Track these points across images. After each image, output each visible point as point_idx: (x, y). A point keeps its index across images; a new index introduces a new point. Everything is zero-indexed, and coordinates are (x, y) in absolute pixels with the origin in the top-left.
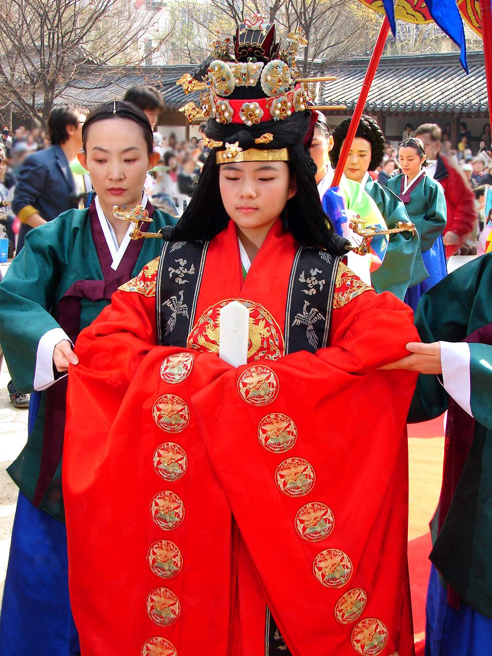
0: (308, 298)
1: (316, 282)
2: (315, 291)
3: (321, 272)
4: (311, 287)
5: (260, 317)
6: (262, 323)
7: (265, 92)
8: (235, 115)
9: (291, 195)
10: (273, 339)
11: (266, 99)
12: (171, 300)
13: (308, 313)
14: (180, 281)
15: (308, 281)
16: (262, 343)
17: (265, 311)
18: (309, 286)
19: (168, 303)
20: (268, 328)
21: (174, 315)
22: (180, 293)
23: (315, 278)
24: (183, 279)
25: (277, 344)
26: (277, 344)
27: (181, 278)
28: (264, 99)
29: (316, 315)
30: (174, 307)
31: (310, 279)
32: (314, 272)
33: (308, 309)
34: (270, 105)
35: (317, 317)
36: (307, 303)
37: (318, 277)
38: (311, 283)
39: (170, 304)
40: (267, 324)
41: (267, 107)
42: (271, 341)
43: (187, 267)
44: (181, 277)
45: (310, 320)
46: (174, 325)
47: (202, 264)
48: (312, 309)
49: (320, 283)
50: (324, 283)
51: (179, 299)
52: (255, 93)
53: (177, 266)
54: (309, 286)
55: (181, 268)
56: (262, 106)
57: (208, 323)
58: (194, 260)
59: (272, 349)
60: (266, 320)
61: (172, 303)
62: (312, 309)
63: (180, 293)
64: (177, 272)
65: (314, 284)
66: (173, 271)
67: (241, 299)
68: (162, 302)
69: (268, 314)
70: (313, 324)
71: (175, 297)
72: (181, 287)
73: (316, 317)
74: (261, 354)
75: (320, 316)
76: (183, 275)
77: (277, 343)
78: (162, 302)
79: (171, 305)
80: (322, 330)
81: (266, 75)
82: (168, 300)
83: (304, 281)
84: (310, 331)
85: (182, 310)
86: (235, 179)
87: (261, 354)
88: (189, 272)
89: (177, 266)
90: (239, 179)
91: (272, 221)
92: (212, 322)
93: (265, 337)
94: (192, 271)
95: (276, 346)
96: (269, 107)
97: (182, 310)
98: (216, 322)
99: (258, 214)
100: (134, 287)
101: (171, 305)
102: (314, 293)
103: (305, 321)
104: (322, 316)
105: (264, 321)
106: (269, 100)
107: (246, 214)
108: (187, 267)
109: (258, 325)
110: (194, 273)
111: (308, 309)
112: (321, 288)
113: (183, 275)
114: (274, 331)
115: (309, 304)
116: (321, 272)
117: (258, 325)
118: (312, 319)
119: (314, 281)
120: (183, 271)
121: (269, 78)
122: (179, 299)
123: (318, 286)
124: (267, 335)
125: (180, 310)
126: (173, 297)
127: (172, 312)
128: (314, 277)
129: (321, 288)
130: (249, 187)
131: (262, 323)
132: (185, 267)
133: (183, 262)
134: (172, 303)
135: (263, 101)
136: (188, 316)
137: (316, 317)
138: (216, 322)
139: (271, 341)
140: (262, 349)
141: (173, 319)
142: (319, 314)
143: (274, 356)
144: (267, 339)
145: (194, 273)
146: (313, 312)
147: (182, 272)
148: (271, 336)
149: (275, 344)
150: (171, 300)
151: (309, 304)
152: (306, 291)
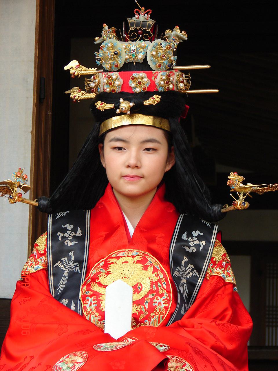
0: (188, 254)
1: (197, 242)
2: (195, 249)
3: (202, 234)
4: (192, 245)
5: (148, 263)
6: (151, 269)
7: (151, 66)
8: (125, 84)
9: (168, 168)
10: (161, 283)
11: (153, 71)
12: (62, 262)
13: (184, 268)
14: (70, 244)
15: (197, 242)
16: (151, 286)
17: (152, 258)
18: (190, 244)
19: (58, 264)
20: (156, 273)
21: (66, 274)
22: (70, 254)
23: (196, 239)
24: (71, 241)
25: (165, 287)
26: (165, 287)
27: (69, 240)
28: (151, 71)
29: (191, 271)
30: (65, 267)
31: (192, 239)
32: (196, 233)
33: (186, 266)
34: (156, 77)
35: (192, 273)
36: (185, 259)
37: (199, 238)
38: (193, 241)
39: (61, 265)
40: (155, 270)
41: (153, 78)
42: (159, 284)
43: (74, 230)
44: (70, 239)
45: (185, 274)
46: (66, 282)
47: (88, 226)
48: (190, 265)
49: (201, 243)
50: (204, 244)
51: (69, 260)
52: (143, 66)
53: (65, 230)
54: (190, 244)
55: (69, 232)
56: (149, 77)
57: (100, 273)
58: (79, 223)
59: (160, 292)
60: (154, 266)
61: (63, 264)
62: (190, 265)
63: (70, 254)
64: (65, 235)
65: (195, 243)
66: (62, 235)
67: (130, 249)
68: (54, 263)
69: (155, 261)
70: (187, 279)
71: (66, 259)
72: (70, 249)
73: (191, 273)
74: (150, 296)
75: (195, 273)
76: (72, 238)
77: (165, 286)
78: (54, 263)
79: (63, 265)
80: (194, 286)
81: (151, 52)
82: (59, 262)
83: (187, 239)
84: (183, 284)
85: (74, 268)
86: (120, 148)
87: (150, 296)
88: (76, 235)
89: (65, 230)
90: (125, 149)
91: (156, 187)
92: (104, 271)
93: (153, 280)
94: (79, 233)
95: (164, 289)
96: (155, 79)
97: (74, 268)
98: (108, 271)
99: (143, 181)
100: (38, 266)
101: (62, 266)
102: (194, 251)
103: (181, 274)
104: (197, 273)
105: (152, 267)
106: (155, 73)
107: (131, 183)
108: (74, 230)
109: (147, 270)
110: (81, 235)
111: (186, 264)
112: (201, 248)
113: (72, 238)
114: (161, 276)
115: (187, 260)
116: (202, 234)
117: (147, 270)
118: (188, 274)
119: (196, 240)
120: (71, 234)
121: (154, 53)
122: (69, 260)
123: (199, 246)
124: (155, 279)
125: (71, 269)
126: (63, 259)
127: (64, 272)
128: (195, 237)
129: (201, 248)
130: (130, 156)
131: (151, 269)
132: (72, 230)
133: (69, 227)
134: (63, 264)
135: (150, 72)
136: (79, 271)
137: (191, 273)
138: (108, 271)
139: (159, 284)
140: (151, 292)
141: (65, 277)
142: (195, 270)
143: (162, 299)
144: (156, 283)
145: (81, 235)
146: (189, 268)
147: (70, 235)
148: (159, 281)
149: (163, 287)
150: (62, 262)
151: (187, 260)
152: (187, 249)
